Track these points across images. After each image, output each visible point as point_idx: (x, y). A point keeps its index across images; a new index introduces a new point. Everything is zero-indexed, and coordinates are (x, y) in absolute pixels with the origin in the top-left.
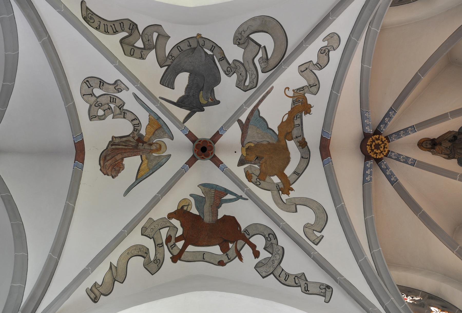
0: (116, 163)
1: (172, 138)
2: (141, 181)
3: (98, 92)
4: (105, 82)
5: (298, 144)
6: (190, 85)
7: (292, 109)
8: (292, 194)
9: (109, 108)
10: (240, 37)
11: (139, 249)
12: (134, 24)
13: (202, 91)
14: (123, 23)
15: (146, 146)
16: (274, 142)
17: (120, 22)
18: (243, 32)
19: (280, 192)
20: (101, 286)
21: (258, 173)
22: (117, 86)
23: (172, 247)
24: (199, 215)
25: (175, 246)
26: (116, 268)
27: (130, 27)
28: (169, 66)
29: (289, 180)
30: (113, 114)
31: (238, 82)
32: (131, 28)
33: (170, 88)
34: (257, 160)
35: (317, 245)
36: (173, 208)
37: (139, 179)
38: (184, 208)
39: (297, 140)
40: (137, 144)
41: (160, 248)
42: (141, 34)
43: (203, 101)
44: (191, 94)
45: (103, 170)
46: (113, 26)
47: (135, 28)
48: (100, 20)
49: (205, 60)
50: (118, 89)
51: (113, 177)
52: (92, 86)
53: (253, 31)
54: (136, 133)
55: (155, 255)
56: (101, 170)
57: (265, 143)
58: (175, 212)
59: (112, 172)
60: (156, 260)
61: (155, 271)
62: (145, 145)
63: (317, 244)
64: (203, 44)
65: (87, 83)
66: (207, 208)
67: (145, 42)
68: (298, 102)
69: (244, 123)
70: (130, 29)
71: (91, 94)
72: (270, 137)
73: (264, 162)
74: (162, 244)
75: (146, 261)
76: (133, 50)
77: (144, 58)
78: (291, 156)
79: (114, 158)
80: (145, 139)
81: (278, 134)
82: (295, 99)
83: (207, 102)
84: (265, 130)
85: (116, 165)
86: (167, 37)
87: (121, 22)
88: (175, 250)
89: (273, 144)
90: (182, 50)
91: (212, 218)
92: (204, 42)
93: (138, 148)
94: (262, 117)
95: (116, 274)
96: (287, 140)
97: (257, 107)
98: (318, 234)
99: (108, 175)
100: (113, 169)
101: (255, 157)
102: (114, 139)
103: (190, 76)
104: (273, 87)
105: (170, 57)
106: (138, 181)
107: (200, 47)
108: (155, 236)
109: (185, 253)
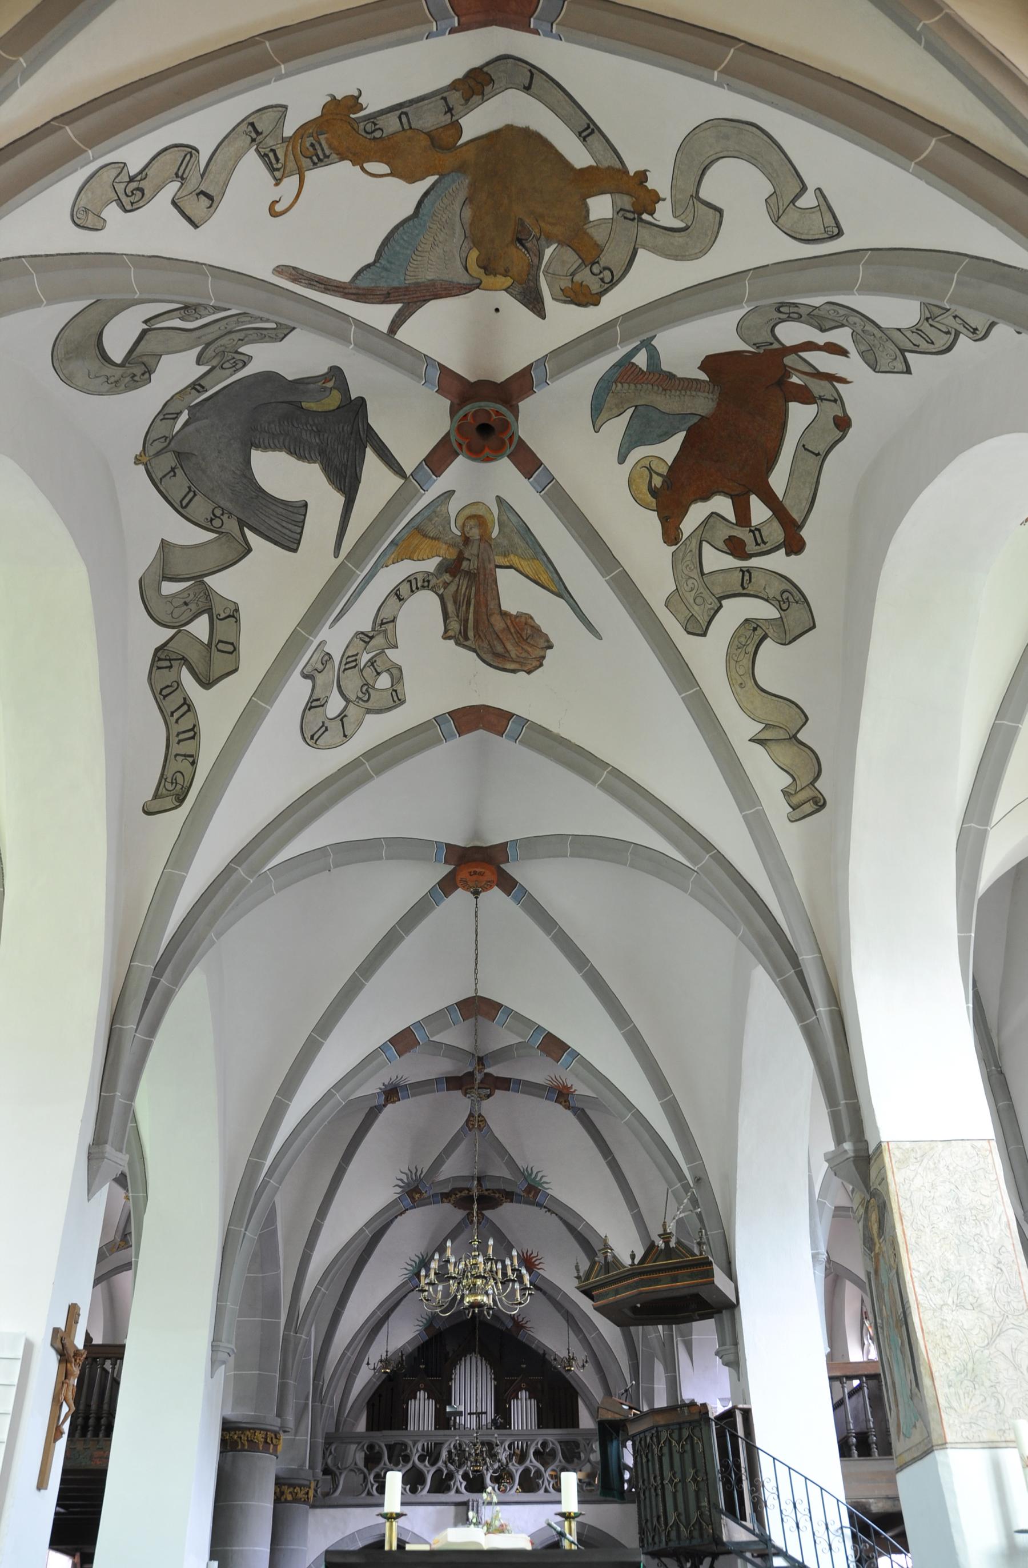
0: (513, 630)
1: (451, 493)
2: (566, 588)
3: (335, 705)
4: (311, 696)
5: (476, 98)
6: (287, 444)
7: (342, 159)
8: (659, 182)
9: (372, 664)
10: (128, 379)
11: (739, 648)
12: (157, 659)
13: (303, 404)
14: (161, 690)
15: (470, 552)
16: (467, 181)
17: (162, 697)
18: (112, 380)
19: (645, 217)
20: (794, 779)
21: (571, 258)
22: (316, 670)
23: (759, 541)
24: (685, 432)
25: (759, 530)
26: (767, 726)
27: (166, 667)
28: (242, 524)
29: (607, 165)
30: (386, 651)
31: (267, 339)
32: (167, 664)
33: (305, 515)
34: (528, 245)
35: (843, 234)
36: (651, 521)
37: (562, 592)
38: (655, 485)
39: (458, 108)
40: (463, 575)
41: (753, 580)
42: (173, 631)
43: (333, 401)
44: (313, 441)
45: (529, 667)
46: (176, 715)
47: (166, 653)
48: (171, 757)
49: (207, 418)
50: (323, 664)
51: (551, 647)
52: (323, 723)
53: (103, 361)
54: (433, 581)
55: (767, 600)
56: (529, 672)
57: (468, 213)
58: (664, 520)
59: (535, 645)
60: (782, 603)
61: (806, 616)
62: (466, 555)
63: (840, 233)
64: (164, 439)
65: (316, 737)
66: (669, 403)
67: (192, 612)
68: (317, 147)
69: (399, 306)
70: (169, 665)
71: (342, 720)
72: (445, 201)
73: (537, 221)
74: (743, 572)
75: (775, 634)
76: (221, 646)
77: (233, 608)
78: (520, 122)
79: (499, 634)
80: (452, 555)
81: (436, 177)
82: (305, 162)
83: (336, 391)
84: (422, 222)
85: (518, 632)
86: (166, 550)
87: (160, 697)
88: (770, 533)
89: (472, 185)
90: (190, 490)
91: (704, 391)
92: (154, 441)
93: (476, 571)
94: (379, 254)
95: (782, 731)
96: (460, 142)
97: (345, 288)
98: (809, 200)
99: (544, 657)
100: (529, 640)
101: (518, 248)
102: (450, 633)
103: (260, 447)
104: (280, 270)
105: (217, 523)
106: (566, 595)
107: (172, 444)
108: (718, 591)
109: (787, 504)
